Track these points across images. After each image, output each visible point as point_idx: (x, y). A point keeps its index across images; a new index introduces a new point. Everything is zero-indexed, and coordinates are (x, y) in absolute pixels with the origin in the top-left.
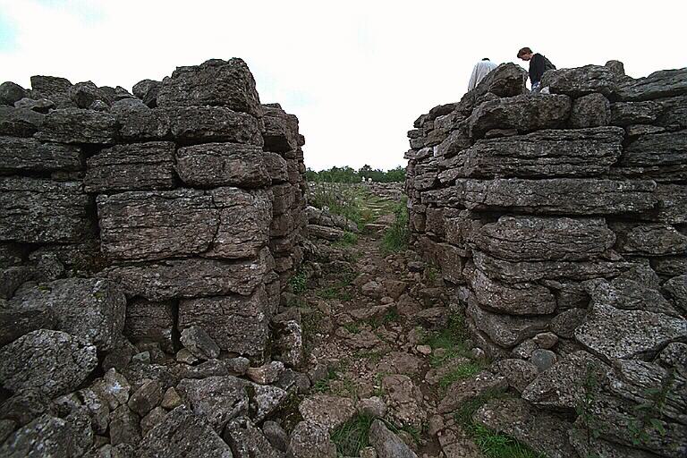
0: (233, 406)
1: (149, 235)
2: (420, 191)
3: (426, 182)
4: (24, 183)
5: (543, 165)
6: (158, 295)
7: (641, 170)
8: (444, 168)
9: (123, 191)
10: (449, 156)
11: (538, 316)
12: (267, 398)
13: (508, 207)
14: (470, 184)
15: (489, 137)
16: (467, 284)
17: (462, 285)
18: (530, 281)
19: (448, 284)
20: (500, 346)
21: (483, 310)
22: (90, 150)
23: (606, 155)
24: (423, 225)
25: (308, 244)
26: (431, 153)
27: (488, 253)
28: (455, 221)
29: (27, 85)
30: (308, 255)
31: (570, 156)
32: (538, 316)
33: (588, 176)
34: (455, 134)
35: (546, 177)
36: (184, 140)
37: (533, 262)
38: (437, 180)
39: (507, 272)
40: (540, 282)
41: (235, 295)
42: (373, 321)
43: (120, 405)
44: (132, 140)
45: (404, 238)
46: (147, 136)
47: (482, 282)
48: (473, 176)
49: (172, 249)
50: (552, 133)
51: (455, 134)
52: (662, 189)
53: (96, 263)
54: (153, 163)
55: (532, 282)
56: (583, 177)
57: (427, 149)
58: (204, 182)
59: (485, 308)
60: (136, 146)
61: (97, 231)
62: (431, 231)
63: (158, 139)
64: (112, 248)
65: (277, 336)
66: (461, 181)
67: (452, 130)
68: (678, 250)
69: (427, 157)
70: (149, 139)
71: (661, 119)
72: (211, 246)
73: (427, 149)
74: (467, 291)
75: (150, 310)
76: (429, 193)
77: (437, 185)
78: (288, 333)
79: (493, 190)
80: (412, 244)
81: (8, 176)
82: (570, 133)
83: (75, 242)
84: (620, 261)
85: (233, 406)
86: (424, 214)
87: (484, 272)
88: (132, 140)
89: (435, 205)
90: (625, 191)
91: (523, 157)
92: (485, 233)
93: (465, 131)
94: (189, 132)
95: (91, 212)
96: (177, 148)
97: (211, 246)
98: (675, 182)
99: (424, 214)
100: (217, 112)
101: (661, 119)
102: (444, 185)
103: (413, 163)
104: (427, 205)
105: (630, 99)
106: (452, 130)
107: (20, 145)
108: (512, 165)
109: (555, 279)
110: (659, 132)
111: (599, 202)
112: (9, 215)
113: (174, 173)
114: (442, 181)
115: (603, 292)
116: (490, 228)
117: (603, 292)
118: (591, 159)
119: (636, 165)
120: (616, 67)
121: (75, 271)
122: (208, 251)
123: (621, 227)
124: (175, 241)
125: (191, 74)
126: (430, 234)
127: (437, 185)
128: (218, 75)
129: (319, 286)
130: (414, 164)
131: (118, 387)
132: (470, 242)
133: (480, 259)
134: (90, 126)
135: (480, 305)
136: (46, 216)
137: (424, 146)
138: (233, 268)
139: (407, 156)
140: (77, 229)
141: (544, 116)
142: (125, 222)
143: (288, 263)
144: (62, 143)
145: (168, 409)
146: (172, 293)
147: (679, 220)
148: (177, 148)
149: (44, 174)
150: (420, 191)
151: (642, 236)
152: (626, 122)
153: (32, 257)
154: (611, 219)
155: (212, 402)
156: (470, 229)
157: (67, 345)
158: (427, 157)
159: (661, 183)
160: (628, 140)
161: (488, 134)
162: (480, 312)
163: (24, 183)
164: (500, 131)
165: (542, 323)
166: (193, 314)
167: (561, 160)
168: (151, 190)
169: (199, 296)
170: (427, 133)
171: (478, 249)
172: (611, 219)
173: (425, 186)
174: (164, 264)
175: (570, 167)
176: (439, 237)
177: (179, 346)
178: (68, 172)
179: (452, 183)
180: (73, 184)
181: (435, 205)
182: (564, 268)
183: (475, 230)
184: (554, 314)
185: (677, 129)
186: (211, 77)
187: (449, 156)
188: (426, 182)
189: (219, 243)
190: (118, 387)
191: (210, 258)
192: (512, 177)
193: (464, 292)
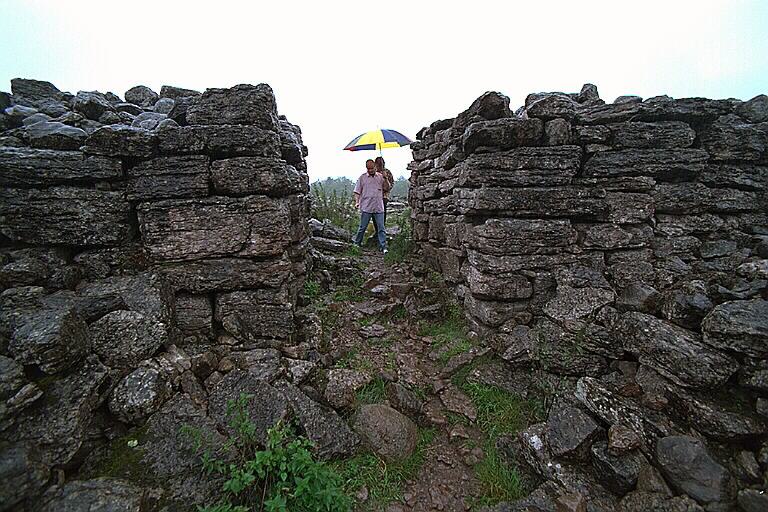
0: (277, 370)
1: (188, 237)
2: (422, 201)
3: (428, 192)
4: (71, 192)
5: (521, 176)
6: (201, 287)
7: (595, 181)
8: (443, 179)
9: (165, 199)
10: (447, 168)
11: (520, 300)
12: (298, 369)
13: (493, 210)
14: (464, 192)
15: (477, 153)
16: (464, 282)
17: (461, 283)
18: (511, 271)
19: (449, 284)
20: (489, 326)
21: (476, 299)
22: (130, 162)
23: (568, 168)
24: (426, 234)
25: (316, 253)
26: (432, 165)
27: (477, 249)
28: (453, 227)
29: (9, 90)
30: (317, 264)
31: (540, 169)
32: (520, 300)
33: (555, 185)
34: (453, 148)
35: (523, 186)
36: (216, 154)
37: (513, 255)
38: (438, 190)
39: (493, 264)
40: (519, 271)
41: (267, 287)
42: (382, 316)
43: (185, 370)
44: (170, 153)
45: (406, 248)
46: (185, 150)
47: (474, 276)
48: (465, 186)
49: (209, 250)
50: (527, 150)
51: (453, 148)
52: (611, 195)
53: (139, 264)
54: (192, 174)
55: (514, 273)
56: (551, 186)
57: (429, 161)
58: (237, 191)
59: (477, 296)
60: (173, 159)
61: (137, 236)
62: (433, 238)
63: (195, 153)
64: (154, 249)
65: (300, 326)
66: (457, 190)
67: (450, 144)
68: (623, 244)
69: (429, 168)
70: (185, 154)
71: (610, 140)
72: (244, 246)
73: (429, 161)
74: (464, 288)
75: (192, 302)
76: (431, 202)
77: (438, 194)
78: (310, 323)
79: (470, 199)
80: (416, 253)
81: (56, 186)
82: (541, 150)
83: (118, 244)
84: (581, 254)
85: (277, 370)
86: (427, 223)
87: (477, 267)
88: (170, 153)
89: (436, 214)
90: (583, 197)
91: (504, 170)
92: (475, 233)
93: (459, 146)
94: (224, 147)
95: (131, 216)
96: (211, 162)
97: (244, 246)
98: (621, 191)
99: (427, 223)
100: (237, 135)
101: (610, 140)
102: (444, 195)
103: (416, 174)
104: (429, 213)
105: (587, 123)
106: (450, 144)
107: (70, 158)
108: (495, 176)
109: (531, 269)
110: (608, 151)
111: (564, 205)
112: (61, 220)
113: (210, 182)
114: (442, 190)
115: (564, 276)
116: (479, 229)
117: (564, 276)
118: (557, 171)
119: (592, 177)
120: (590, 91)
121: (121, 270)
122: (241, 251)
123: (581, 227)
124: (212, 243)
125: (222, 96)
126: (433, 241)
127: (438, 194)
128: (248, 99)
129: (330, 291)
130: (417, 176)
131: (180, 358)
132: (465, 242)
133: (472, 255)
134: (134, 142)
135: (474, 295)
136: (93, 222)
137: (426, 158)
138: (265, 264)
139: (409, 167)
140: (122, 232)
141: (521, 135)
142: (168, 227)
143: (302, 267)
144: (106, 156)
145: (223, 373)
146: (214, 285)
147: (623, 220)
148: (211, 162)
149: (87, 182)
150: (422, 201)
151: (595, 232)
152: (584, 142)
153: (78, 259)
154: (576, 219)
155: (259, 367)
156: (465, 231)
157: (142, 321)
158: (429, 168)
159: (611, 191)
160: (586, 156)
161: (477, 150)
162: (474, 301)
163: (71, 192)
164: (484, 148)
165: (521, 306)
166: (231, 304)
167: (534, 172)
168: (191, 198)
169: (236, 289)
170: (428, 145)
171: (471, 248)
172: (576, 219)
173: (427, 195)
174: (201, 263)
175: (540, 177)
176: (441, 242)
177: (218, 327)
178: (113, 182)
179: (450, 192)
180: (116, 193)
181: (436, 214)
182: (538, 260)
183: (468, 233)
184: (531, 298)
185: (621, 149)
186: (242, 99)
187: (447, 168)
188: (428, 192)
189: (251, 243)
190: (180, 358)
191: (243, 257)
192: (495, 186)
193: (462, 289)
